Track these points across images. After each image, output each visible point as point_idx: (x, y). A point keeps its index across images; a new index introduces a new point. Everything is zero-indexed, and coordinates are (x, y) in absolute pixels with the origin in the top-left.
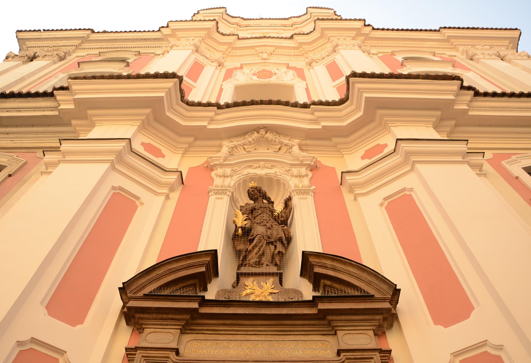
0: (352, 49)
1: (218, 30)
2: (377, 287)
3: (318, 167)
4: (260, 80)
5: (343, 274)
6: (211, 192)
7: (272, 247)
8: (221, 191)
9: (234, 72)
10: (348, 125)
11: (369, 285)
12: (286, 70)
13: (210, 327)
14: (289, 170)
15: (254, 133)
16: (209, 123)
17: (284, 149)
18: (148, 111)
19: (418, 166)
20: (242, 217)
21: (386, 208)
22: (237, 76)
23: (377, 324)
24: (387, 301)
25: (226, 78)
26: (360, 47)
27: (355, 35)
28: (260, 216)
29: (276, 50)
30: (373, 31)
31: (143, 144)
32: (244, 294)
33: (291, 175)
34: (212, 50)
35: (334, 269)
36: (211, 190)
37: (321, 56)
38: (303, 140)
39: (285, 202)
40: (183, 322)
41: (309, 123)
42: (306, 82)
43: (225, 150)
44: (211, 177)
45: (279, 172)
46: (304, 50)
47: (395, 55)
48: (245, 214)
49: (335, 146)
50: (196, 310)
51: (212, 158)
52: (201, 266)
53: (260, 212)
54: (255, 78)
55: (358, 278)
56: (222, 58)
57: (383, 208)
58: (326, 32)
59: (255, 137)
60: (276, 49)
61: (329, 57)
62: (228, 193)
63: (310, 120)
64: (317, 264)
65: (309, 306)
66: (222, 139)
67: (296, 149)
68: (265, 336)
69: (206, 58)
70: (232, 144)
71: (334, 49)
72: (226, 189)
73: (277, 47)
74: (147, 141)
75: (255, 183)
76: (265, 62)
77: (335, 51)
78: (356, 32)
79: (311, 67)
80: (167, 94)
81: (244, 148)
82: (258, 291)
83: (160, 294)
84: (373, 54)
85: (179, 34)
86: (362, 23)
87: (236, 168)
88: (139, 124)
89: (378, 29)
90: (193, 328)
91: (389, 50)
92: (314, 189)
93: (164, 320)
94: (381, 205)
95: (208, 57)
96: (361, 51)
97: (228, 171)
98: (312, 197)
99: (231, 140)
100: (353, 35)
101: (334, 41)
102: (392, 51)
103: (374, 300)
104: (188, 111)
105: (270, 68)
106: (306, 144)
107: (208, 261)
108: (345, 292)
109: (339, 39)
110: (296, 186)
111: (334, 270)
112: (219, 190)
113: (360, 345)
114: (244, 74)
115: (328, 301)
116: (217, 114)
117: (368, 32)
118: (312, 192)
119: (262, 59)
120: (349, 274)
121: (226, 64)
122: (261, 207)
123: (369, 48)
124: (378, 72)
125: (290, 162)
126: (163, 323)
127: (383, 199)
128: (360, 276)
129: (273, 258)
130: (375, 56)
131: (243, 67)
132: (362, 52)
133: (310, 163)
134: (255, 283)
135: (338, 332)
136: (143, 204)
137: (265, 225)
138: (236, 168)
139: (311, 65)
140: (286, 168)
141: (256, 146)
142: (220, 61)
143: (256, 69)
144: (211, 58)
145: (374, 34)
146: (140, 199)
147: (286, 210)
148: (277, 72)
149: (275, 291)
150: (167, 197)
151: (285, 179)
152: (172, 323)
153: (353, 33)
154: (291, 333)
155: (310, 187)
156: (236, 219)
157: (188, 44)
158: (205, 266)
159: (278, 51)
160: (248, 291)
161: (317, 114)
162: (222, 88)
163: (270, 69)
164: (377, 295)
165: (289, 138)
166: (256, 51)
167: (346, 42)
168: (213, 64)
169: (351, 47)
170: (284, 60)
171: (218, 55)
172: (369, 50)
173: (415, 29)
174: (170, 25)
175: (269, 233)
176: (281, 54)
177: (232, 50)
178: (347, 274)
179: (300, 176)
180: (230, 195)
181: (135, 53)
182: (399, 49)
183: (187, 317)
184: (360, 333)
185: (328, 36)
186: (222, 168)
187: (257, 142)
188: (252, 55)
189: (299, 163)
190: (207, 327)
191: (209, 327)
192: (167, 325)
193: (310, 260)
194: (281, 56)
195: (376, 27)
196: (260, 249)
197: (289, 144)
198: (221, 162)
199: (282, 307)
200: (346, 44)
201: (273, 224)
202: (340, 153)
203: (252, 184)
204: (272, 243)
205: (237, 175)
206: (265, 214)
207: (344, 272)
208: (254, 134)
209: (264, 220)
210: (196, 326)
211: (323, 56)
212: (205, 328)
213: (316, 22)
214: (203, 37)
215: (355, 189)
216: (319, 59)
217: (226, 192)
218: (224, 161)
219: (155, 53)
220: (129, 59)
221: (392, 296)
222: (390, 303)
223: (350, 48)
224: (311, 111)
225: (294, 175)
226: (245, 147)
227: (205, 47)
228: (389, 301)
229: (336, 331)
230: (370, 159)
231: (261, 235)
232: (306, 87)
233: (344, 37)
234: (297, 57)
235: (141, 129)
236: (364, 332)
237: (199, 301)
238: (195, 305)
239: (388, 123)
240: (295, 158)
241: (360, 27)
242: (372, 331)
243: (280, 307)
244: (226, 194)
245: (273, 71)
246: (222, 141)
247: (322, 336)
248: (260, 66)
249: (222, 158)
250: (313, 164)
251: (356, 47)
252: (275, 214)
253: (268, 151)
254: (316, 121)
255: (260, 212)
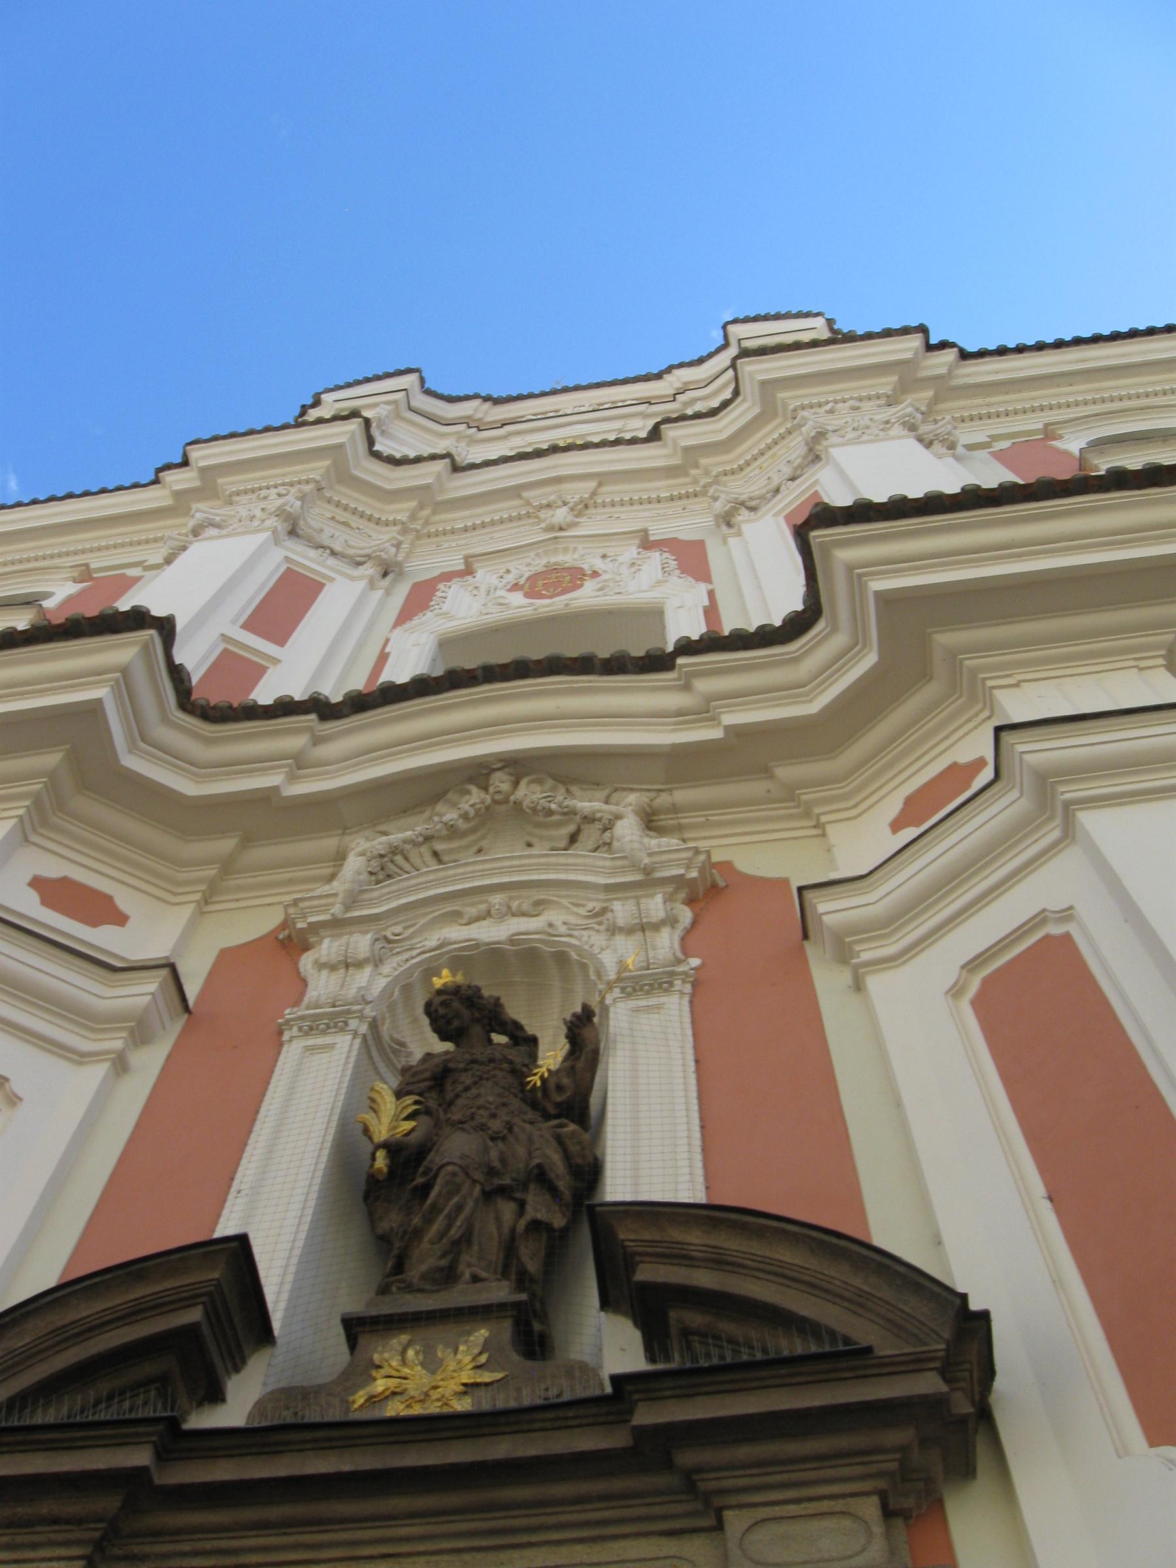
0: (888, 439)
1: (375, 449)
2: (892, 1316)
3: (722, 884)
4: (531, 604)
5: (753, 1277)
6: (291, 1029)
7: (507, 1209)
8: (326, 1021)
9: (438, 590)
10: (825, 710)
11: (860, 1311)
12: (635, 555)
13: (208, 1539)
14: (604, 910)
15: (469, 792)
16: (292, 778)
17: (590, 835)
18: (51, 759)
19: (1088, 819)
20: (393, 1106)
21: (975, 1003)
22: (447, 601)
23: (894, 1466)
24: (932, 1365)
25: (405, 615)
26: (912, 428)
27: (894, 390)
28: (469, 1094)
29: (604, 489)
30: (929, 354)
31: (37, 883)
32: (362, 1401)
33: (607, 930)
34: (354, 521)
35: (719, 1262)
36: (288, 1022)
37: (767, 485)
38: (661, 790)
39: (569, 1029)
40: (96, 1529)
41: (676, 724)
42: (710, 587)
43: (354, 865)
44: (298, 973)
45: (565, 923)
46: (707, 473)
47: (1060, 437)
48: (409, 1093)
49: (790, 794)
50: (139, 1475)
51: (301, 905)
52: (184, 1303)
53: (467, 1079)
54: (517, 599)
55: (814, 1287)
56: (393, 545)
57: (965, 1005)
58: (781, 395)
59: (472, 806)
60: (600, 485)
61: (797, 482)
62: (353, 1024)
63: (680, 713)
64: (649, 1250)
65: (602, 1419)
66: (347, 831)
67: (628, 830)
68: (427, 1558)
69: (333, 553)
70: (379, 843)
71: (811, 450)
72: (348, 1012)
73: (603, 479)
74: (53, 869)
75: (454, 974)
76: (556, 538)
77: (818, 458)
78: (895, 378)
79: (731, 531)
80: (116, 688)
81: (436, 854)
82: (417, 1378)
83: (28, 1422)
84: (970, 447)
85: (228, 484)
86: (915, 342)
87: (398, 929)
88: (21, 812)
89: (982, 354)
90: (137, 1549)
91: (1034, 423)
92: (692, 969)
93: (20, 1526)
94: (955, 992)
95: (338, 548)
96: (916, 443)
97: (362, 943)
98: (686, 1000)
99: (383, 828)
100: (886, 390)
101: (809, 420)
102: (1046, 425)
103: (875, 1366)
104: (208, 741)
105: (576, 556)
106: (674, 804)
107: (215, 1282)
108: (765, 1351)
109: (833, 413)
110: (622, 966)
111: (716, 1267)
112: (316, 1017)
113: (818, 1561)
114: (475, 592)
115: (678, 1392)
116: (317, 741)
117: (944, 370)
118: (684, 981)
119: (550, 528)
120: (776, 1274)
121: (409, 566)
122: (474, 1061)
123: (949, 427)
124: (915, 492)
125: (602, 881)
126: (19, 1539)
127: (963, 967)
128: (821, 1276)
129: (510, 1248)
130: (983, 454)
131: (476, 565)
132: (919, 447)
133: (682, 871)
134: (411, 1353)
135: (728, 1515)
136: (15, 1100)
137: (482, 1127)
138: (398, 929)
139: (733, 521)
140: (590, 906)
141: (483, 838)
142: (384, 556)
143: (522, 568)
144: (351, 552)
145: (968, 376)
146: (7, 1085)
147: (578, 1058)
148: (599, 564)
149: (487, 1377)
150: (120, 1065)
151: (586, 947)
152: (53, 1536)
153: (886, 384)
154: (534, 1538)
155: (679, 962)
156: (369, 1117)
157: (258, 513)
158: (203, 1303)
159: (610, 492)
160: (380, 1385)
161: (704, 686)
162: (387, 650)
163: (575, 560)
164: (886, 1347)
165: (606, 792)
166: (528, 503)
167: (856, 419)
168: (361, 571)
169: (876, 432)
170: (632, 519)
171: (380, 540)
172: (948, 434)
173: (1124, 329)
174: (195, 453)
175: (494, 1154)
176: (631, 499)
177: (434, 513)
178: (771, 1277)
179: (643, 927)
180: (364, 1028)
181: (72, 572)
182: (1068, 413)
183: (109, 1504)
184: (821, 1514)
185: (792, 407)
186: (341, 935)
187: (484, 818)
188: (510, 519)
189: (638, 877)
190: (192, 1540)
191: (200, 1540)
192: (35, 1546)
193: (622, 1236)
194: (623, 509)
195: (972, 348)
196: (451, 1220)
197: (598, 815)
198: (333, 915)
199: (491, 1434)
200: (856, 425)
201: (516, 1120)
202: (813, 823)
203: (444, 979)
204: (503, 1191)
205: (398, 953)
206: (489, 1084)
207: (758, 1270)
208: (468, 796)
209: (479, 1108)
210: (151, 1543)
211: (775, 483)
212: (186, 1547)
213: (738, 366)
214: (317, 482)
215: (857, 948)
216: (762, 498)
217: (346, 1024)
218: (348, 908)
219: (145, 561)
220: (47, 595)
221: (948, 1343)
222: (945, 1374)
223: (873, 437)
224: (679, 679)
225: (619, 927)
226: (439, 847)
227: (329, 515)
228: (937, 1364)
229: (719, 1511)
230: (918, 825)
231: (454, 1164)
232: (706, 603)
233: (851, 403)
234: (684, 502)
235: (34, 830)
236: (839, 1505)
237: (154, 1438)
238: (140, 1457)
239: (984, 679)
240: (625, 862)
241: (908, 355)
242: (875, 1500)
243: (484, 1435)
244: (348, 1028)
245: (586, 567)
246: (347, 838)
247: (664, 1541)
248: (537, 555)
249: (340, 899)
250: (694, 874)
251: (897, 430)
252: (530, 1082)
253: (528, 851)
254: (704, 713)
255: (468, 1082)
